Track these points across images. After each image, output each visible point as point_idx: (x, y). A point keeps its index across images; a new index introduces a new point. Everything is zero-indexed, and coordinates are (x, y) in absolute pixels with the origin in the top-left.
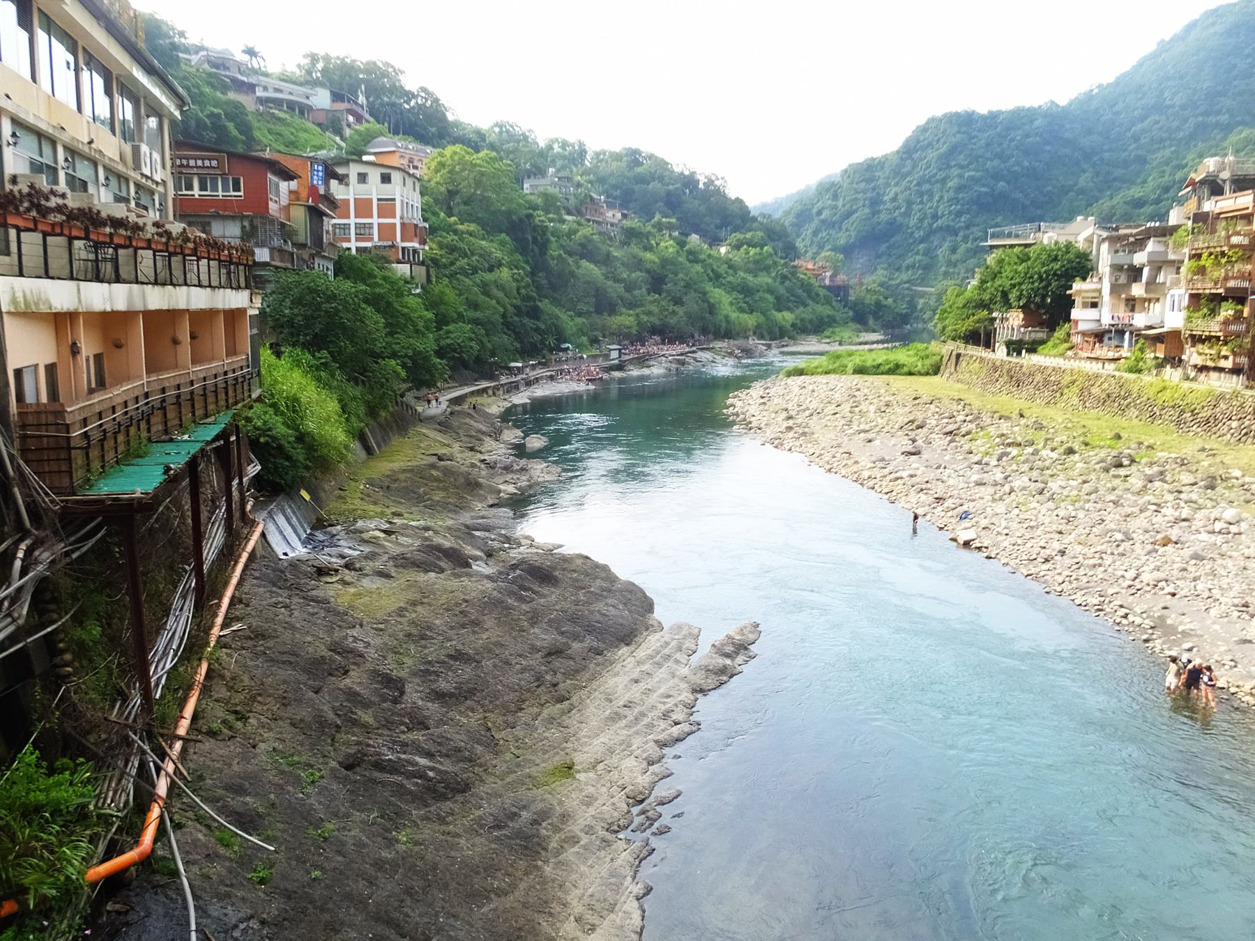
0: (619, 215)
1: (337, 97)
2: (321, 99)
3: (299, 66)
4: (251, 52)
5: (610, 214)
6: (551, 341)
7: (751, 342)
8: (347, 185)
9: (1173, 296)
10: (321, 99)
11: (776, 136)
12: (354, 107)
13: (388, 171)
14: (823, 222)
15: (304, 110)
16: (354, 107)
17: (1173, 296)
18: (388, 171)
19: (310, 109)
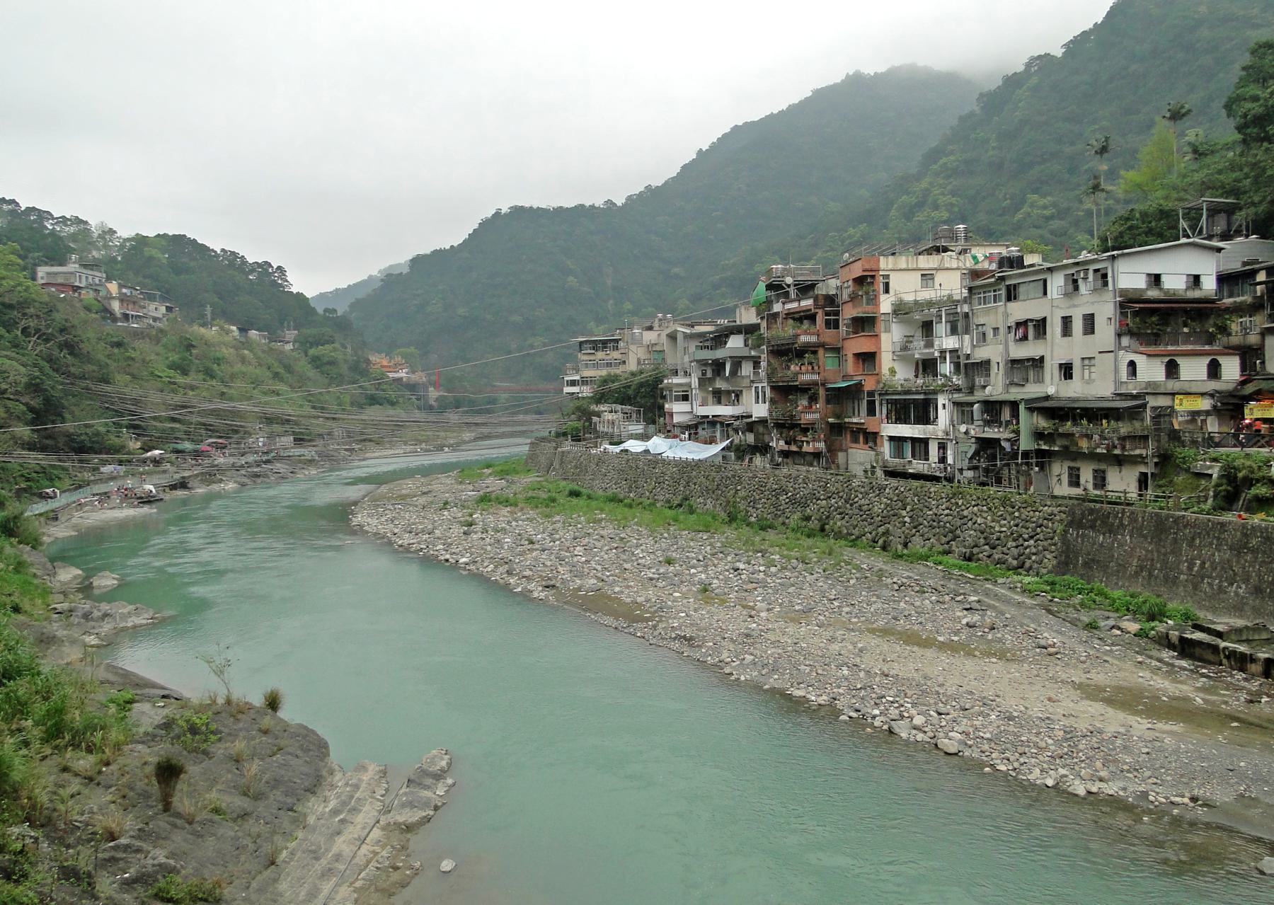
6: (720, 384)
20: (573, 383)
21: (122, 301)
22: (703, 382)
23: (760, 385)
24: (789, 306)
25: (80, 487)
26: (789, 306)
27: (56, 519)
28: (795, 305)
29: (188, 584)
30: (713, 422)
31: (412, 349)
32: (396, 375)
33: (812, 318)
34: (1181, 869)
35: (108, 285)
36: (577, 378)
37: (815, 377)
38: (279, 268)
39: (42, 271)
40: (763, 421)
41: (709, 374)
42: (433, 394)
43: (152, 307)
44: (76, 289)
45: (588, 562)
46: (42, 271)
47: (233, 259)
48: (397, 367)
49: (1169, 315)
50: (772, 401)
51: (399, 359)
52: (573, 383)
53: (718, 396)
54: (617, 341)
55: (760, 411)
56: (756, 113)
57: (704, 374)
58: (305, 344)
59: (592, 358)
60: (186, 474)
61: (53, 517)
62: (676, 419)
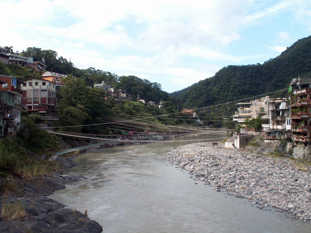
0: (125, 95)
1: (35, 60)
2: (30, 60)
3: (304, 148)
4: (18, 51)
5: (122, 95)
6: (279, 119)
7: (262, 117)
8: (26, 86)
9: (288, 120)
10: (30, 60)
11: (175, 77)
12: (41, 63)
13: (45, 81)
14: (193, 97)
15: (24, 64)
16: (41, 63)
17: (288, 120)
18: (45, 81)
19: (26, 63)
20: (236, 118)
22: (273, 118)
23: (289, 119)
24: (298, 92)
25: (195, 213)
26: (298, 92)
27: (86, 151)
28: (300, 92)
29: (87, 164)
30: (276, 131)
33: (306, 96)
34: (218, 191)
36: (238, 116)
37: (307, 116)
40: (289, 131)
41: (275, 115)
50: (292, 125)
52: (236, 118)
53: (278, 123)
55: (288, 127)
56: (233, 65)
57: (273, 115)
62: (264, 130)
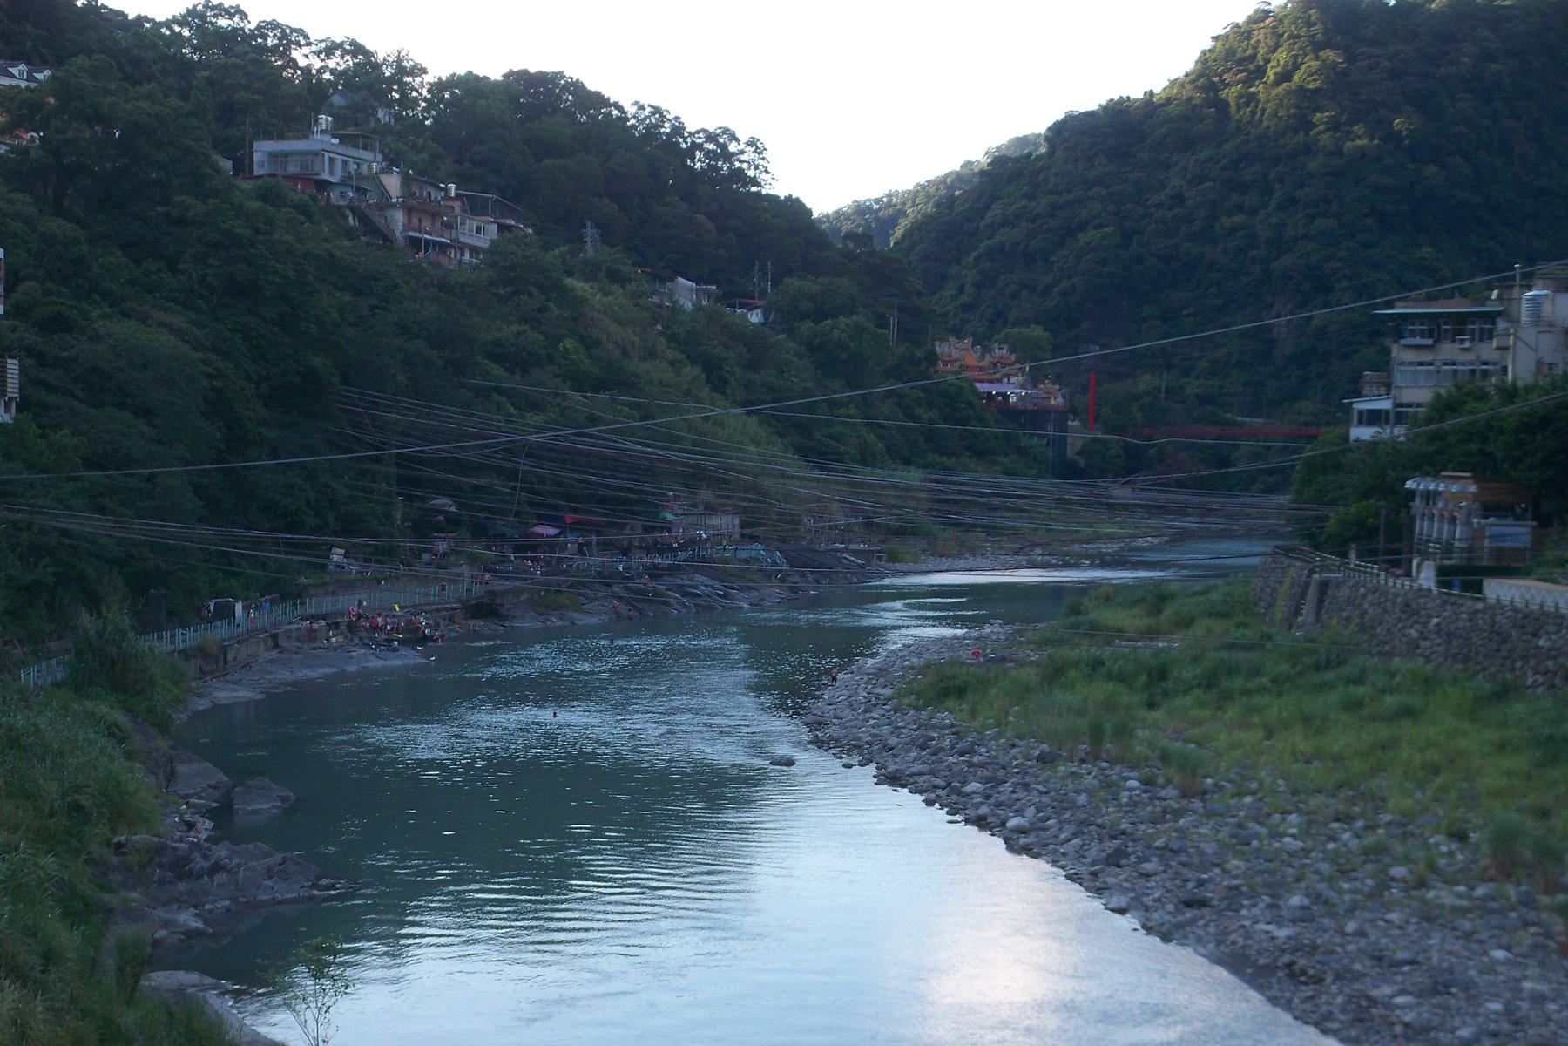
20: (1373, 418)
21: (409, 211)
31: (1037, 332)
32: (994, 389)
35: (385, 179)
36: (1385, 404)
38: (752, 143)
39: (262, 150)
42: (1078, 435)
43: (472, 223)
44: (323, 185)
45: (1306, 852)
46: (262, 150)
47: (486, 78)
48: (995, 371)
49: (480, 606)
51: (1000, 352)
52: (1373, 418)
54: (1491, 317)
58: (785, 316)
59: (1425, 356)
60: (499, 586)
61: (214, 661)
